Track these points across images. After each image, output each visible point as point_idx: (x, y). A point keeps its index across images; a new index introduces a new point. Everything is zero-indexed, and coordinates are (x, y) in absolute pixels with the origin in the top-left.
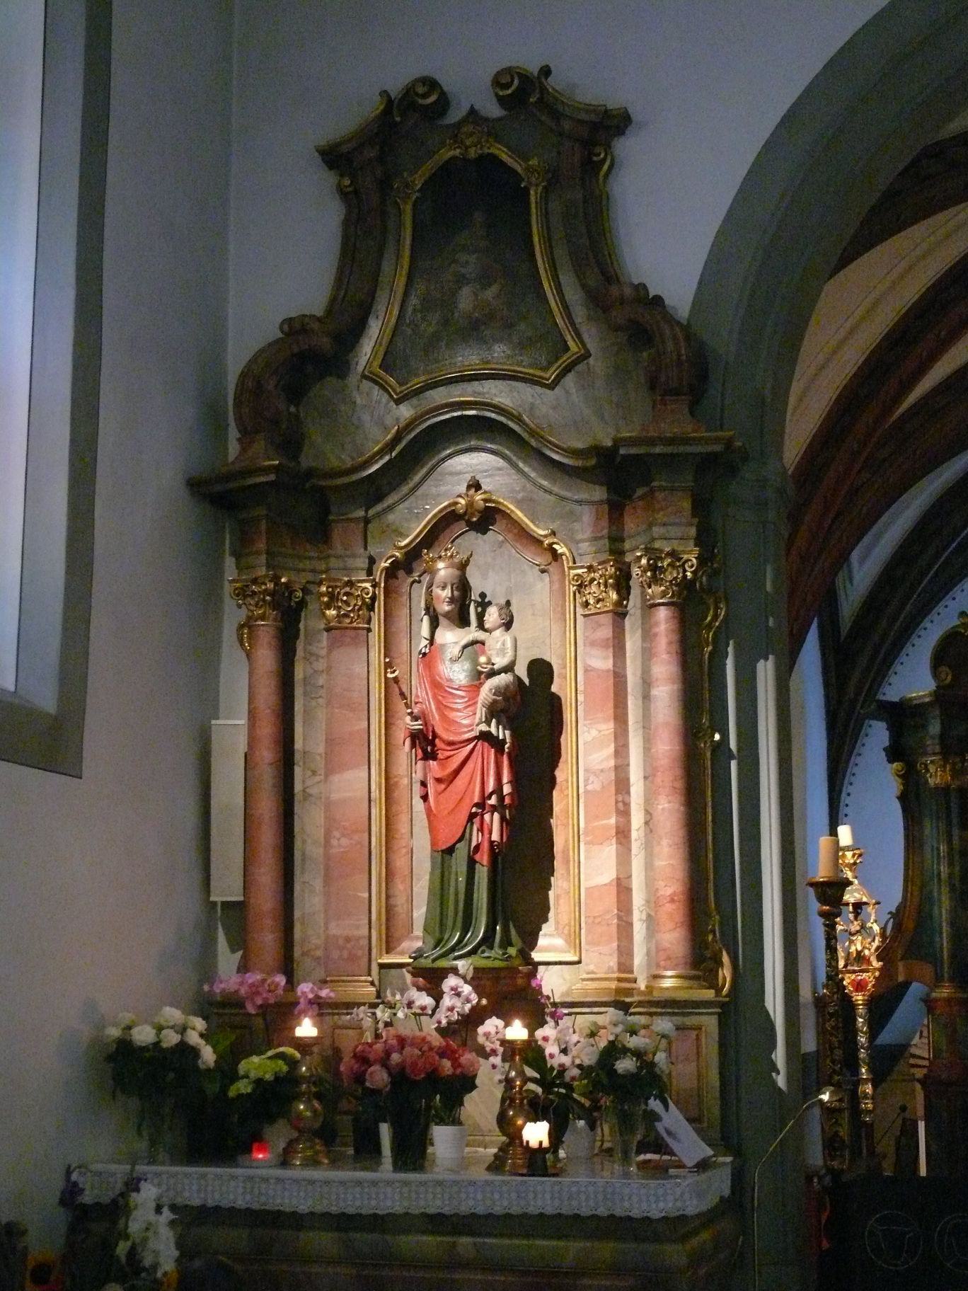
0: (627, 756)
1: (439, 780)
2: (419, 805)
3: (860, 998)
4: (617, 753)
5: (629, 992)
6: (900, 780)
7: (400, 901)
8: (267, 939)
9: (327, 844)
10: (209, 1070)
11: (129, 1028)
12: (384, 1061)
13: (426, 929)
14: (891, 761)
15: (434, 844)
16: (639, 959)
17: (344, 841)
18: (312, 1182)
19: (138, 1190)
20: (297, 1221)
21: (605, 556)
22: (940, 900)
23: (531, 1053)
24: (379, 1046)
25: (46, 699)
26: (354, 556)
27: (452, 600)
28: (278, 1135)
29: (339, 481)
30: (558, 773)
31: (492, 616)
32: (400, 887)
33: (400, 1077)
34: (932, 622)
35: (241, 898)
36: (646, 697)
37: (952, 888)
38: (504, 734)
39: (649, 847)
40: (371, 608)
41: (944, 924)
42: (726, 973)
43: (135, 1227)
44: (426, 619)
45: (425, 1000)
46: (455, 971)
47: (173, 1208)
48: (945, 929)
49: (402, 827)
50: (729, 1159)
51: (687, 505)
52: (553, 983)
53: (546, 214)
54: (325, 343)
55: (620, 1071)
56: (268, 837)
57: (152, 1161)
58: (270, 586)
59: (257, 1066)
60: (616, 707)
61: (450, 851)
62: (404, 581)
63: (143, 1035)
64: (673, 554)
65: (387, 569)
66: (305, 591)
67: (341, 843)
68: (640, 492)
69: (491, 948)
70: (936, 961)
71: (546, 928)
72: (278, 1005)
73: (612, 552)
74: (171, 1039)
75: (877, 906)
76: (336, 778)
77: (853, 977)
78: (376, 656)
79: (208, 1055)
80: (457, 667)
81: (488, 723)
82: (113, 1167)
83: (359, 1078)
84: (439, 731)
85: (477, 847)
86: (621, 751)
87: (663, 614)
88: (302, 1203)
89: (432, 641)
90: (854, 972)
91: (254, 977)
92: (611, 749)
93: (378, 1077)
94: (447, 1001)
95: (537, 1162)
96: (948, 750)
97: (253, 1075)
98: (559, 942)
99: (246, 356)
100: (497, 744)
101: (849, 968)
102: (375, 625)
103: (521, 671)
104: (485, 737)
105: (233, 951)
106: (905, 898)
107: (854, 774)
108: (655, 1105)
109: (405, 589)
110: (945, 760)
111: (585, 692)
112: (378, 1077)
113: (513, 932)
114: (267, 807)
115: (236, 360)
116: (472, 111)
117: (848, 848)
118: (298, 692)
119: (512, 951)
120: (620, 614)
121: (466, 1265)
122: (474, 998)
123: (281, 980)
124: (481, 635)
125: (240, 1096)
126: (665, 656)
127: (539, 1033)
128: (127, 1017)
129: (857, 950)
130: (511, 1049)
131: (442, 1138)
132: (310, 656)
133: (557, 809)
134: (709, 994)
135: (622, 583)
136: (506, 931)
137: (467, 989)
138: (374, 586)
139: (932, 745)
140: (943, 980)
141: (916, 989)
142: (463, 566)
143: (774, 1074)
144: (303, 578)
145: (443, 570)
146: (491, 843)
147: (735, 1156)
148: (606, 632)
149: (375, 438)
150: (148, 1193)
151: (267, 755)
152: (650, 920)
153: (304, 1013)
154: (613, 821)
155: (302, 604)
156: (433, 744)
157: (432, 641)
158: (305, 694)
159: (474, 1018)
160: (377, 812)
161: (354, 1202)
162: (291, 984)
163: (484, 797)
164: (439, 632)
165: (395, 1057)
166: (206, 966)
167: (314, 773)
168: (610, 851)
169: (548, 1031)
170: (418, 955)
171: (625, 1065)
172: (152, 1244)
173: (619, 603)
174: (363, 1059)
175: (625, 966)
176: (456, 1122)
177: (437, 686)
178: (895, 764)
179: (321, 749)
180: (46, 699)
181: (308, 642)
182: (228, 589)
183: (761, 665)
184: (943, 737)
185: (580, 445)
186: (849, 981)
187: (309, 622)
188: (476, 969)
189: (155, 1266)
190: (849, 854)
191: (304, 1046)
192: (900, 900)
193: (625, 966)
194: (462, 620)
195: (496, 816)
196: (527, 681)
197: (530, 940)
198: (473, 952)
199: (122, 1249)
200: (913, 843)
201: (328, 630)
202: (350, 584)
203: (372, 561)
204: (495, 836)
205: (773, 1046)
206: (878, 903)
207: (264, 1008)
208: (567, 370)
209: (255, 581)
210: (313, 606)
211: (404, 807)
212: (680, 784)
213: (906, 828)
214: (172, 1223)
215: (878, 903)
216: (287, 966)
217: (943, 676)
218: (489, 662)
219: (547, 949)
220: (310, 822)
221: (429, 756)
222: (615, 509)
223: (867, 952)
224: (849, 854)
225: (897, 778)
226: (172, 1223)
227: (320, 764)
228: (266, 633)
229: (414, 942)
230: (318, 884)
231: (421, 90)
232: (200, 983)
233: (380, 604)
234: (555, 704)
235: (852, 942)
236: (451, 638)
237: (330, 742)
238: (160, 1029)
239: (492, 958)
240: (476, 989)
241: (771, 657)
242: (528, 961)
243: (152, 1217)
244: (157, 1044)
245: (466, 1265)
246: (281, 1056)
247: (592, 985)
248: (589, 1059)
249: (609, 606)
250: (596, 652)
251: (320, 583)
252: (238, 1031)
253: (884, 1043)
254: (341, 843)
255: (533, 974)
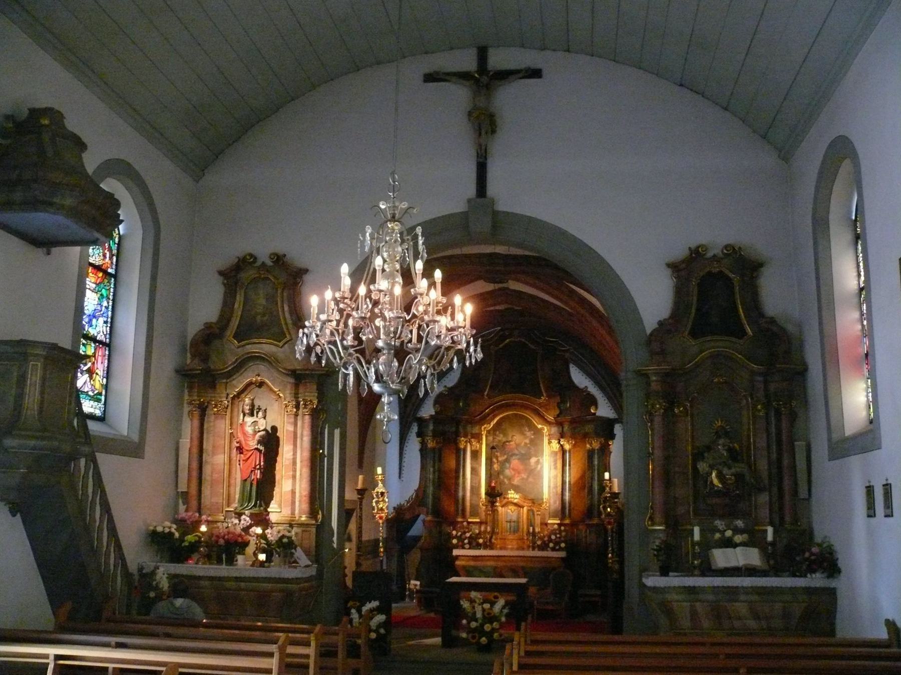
0: (296, 455)
1: (243, 460)
2: (238, 466)
4: (294, 454)
5: (293, 521)
7: (232, 492)
8: (194, 503)
9: (212, 476)
10: (177, 539)
11: (155, 527)
12: (223, 538)
13: (239, 501)
15: (241, 477)
16: (297, 512)
17: (216, 475)
18: (204, 568)
19: (158, 569)
20: (200, 578)
21: (293, 399)
23: (263, 536)
24: (222, 534)
25: (135, 437)
26: (222, 393)
27: (249, 410)
28: (195, 556)
29: (219, 372)
30: (278, 458)
31: (260, 414)
32: (232, 488)
33: (227, 542)
35: (186, 490)
36: (302, 439)
37: (434, 484)
38: (262, 448)
39: (301, 480)
40: (227, 408)
42: (320, 516)
43: (158, 577)
44: (242, 414)
45: (236, 521)
46: (244, 514)
47: (168, 574)
48: (431, 496)
49: (233, 471)
50: (316, 566)
51: (315, 387)
52: (273, 518)
53: (282, 297)
54: (217, 331)
56: (195, 474)
57: (161, 562)
58: (198, 402)
59: (190, 538)
60: (294, 441)
61: (246, 480)
62: (236, 401)
63: (160, 529)
64: (311, 401)
65: (232, 397)
66: (208, 403)
67: (215, 476)
68: (303, 381)
69: (256, 507)
70: (428, 508)
71: (272, 502)
72: (196, 521)
73: (295, 397)
74: (167, 530)
76: (215, 457)
78: (228, 422)
79: (177, 535)
80: (250, 428)
81: (258, 445)
82: (152, 564)
83: (217, 542)
84: (244, 446)
85: (253, 480)
86: (295, 454)
87: (307, 417)
88: (201, 573)
89: (243, 420)
91: (190, 514)
92: (292, 453)
93: (222, 542)
94: (242, 522)
95: (262, 564)
96: (435, 435)
97: (189, 540)
98: (276, 506)
99: (194, 332)
100: (260, 451)
102: (228, 413)
103: (269, 429)
104: (257, 449)
105: (184, 505)
108: (293, 551)
109: (237, 403)
111: (286, 436)
112: (222, 542)
113: (262, 502)
114: (195, 465)
115: (189, 338)
116: (263, 262)
118: (205, 431)
119: (262, 508)
120: (296, 415)
121: (243, 590)
122: (250, 521)
123: (197, 515)
124: (257, 419)
125: (185, 546)
126: (307, 429)
127: (266, 531)
128: (155, 524)
130: (258, 536)
131: (240, 558)
132: (209, 422)
133: (277, 468)
134: (314, 522)
135: (297, 407)
136: (260, 503)
137: (248, 519)
138: (228, 402)
142: (253, 400)
144: (208, 399)
145: (247, 401)
146: (257, 479)
147: (318, 565)
148: (292, 420)
149: (231, 359)
150: (161, 569)
151: (195, 451)
152: (300, 501)
153: (203, 524)
154: (291, 473)
155: (207, 407)
156: (242, 449)
157: (243, 420)
158: (207, 433)
159: (250, 526)
160: (226, 467)
161: (212, 573)
162: (200, 515)
163: (256, 466)
164: (245, 417)
165: (226, 537)
166: (176, 511)
167: (209, 455)
168: (290, 482)
169: (268, 531)
170: (236, 508)
171: (285, 540)
172: (162, 582)
173: (296, 412)
174: (218, 537)
175: (293, 513)
176: (244, 554)
177: (244, 434)
179: (211, 449)
180: (135, 437)
181: (208, 418)
182: (186, 402)
183: (336, 431)
184: (434, 431)
185: (289, 368)
187: (208, 412)
188: (251, 513)
189: (163, 588)
190: (380, 476)
191: (202, 533)
193: (293, 513)
194: (252, 415)
195: (259, 471)
196: (270, 432)
197: (268, 505)
198: (251, 508)
199: (154, 583)
200: (423, 468)
201: (214, 414)
202: (221, 401)
203: (228, 395)
204: (258, 477)
205: (333, 536)
207: (192, 523)
208: (286, 343)
209: (194, 400)
210: (210, 407)
211: (234, 466)
212: (309, 464)
214: (167, 578)
216: (199, 510)
218: (259, 428)
219: (272, 508)
220: (207, 470)
221: (241, 453)
222: (297, 386)
226: (167, 578)
227: (211, 453)
228: (197, 414)
229: (235, 505)
230: (209, 487)
231: (248, 257)
232: (174, 515)
233: (230, 407)
234: (277, 440)
236: (249, 420)
237: (214, 447)
238: (164, 528)
239: (256, 510)
240: (251, 519)
242: (266, 511)
243: (162, 575)
244: (163, 532)
245: (243, 590)
246: (196, 535)
247: (283, 518)
248: (277, 539)
249: (294, 413)
250: (289, 425)
251: (212, 401)
254: (215, 476)
255: (268, 515)
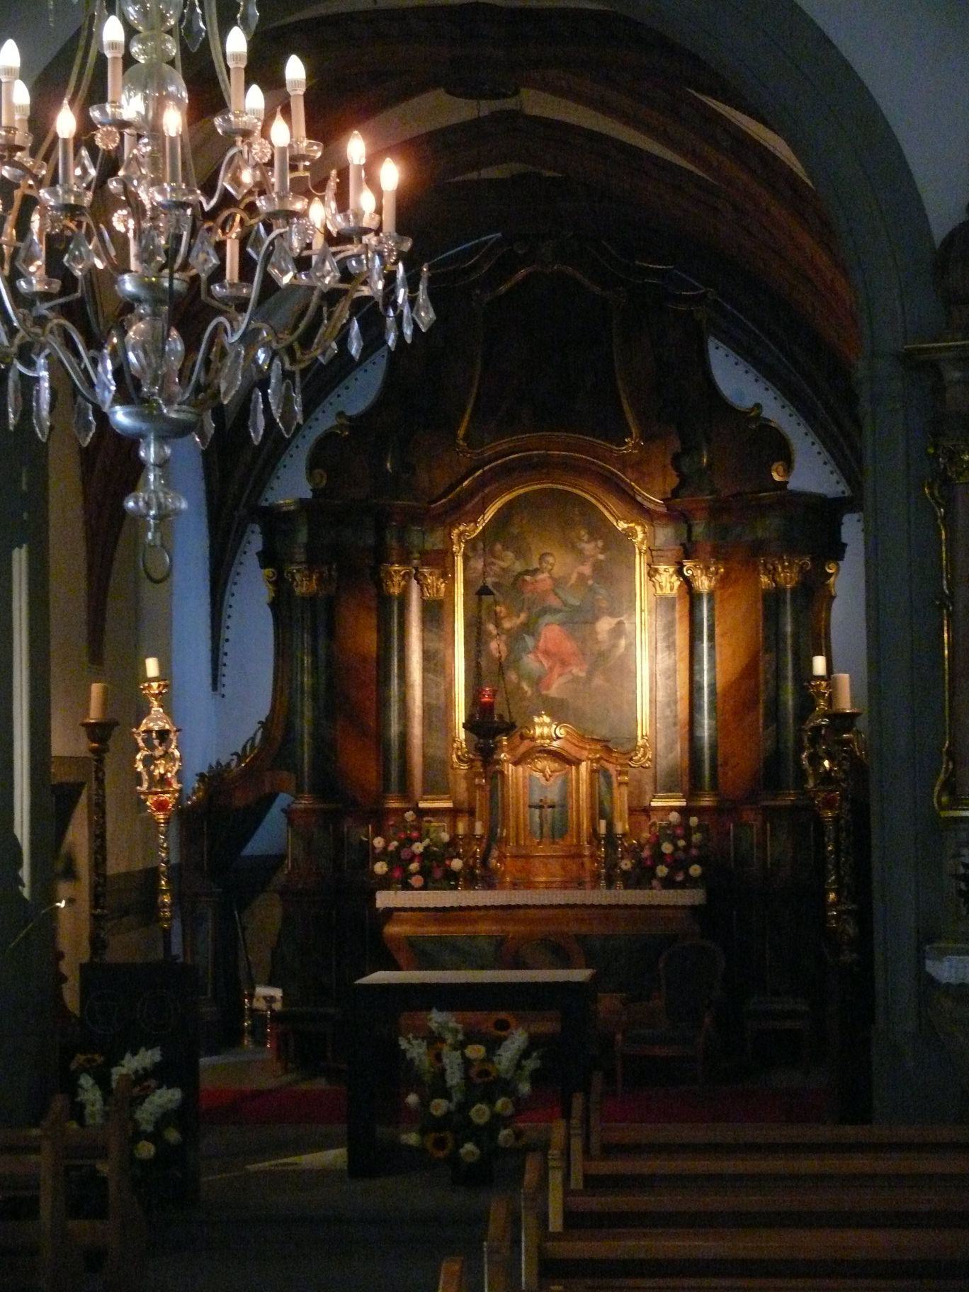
3: (162, 817)
6: (271, 587)
14: (263, 566)
22: (302, 713)
34: (324, 412)
37: (315, 698)
41: (306, 736)
48: (307, 739)
55: (942, 816)
75: (178, 733)
77: (155, 798)
90: (156, 793)
96: (312, 562)
101: (154, 789)
106: (273, 709)
107: (238, 574)
110: (311, 571)
117: (154, 679)
125: (966, 886)
129: (160, 773)
139: (300, 555)
140: (302, 792)
141: (283, 800)
143: (20, 887)
178: (267, 570)
184: (309, 549)
186: (151, 801)
190: (155, 685)
192: (267, 713)
205: (20, 864)
206: (178, 731)
213: (277, 637)
215: (178, 731)
217: (318, 480)
223: (169, 775)
224: (155, 685)
225: (268, 584)
235: (156, 765)
241: (25, 545)
252: (298, 251)
253: (258, 853)
